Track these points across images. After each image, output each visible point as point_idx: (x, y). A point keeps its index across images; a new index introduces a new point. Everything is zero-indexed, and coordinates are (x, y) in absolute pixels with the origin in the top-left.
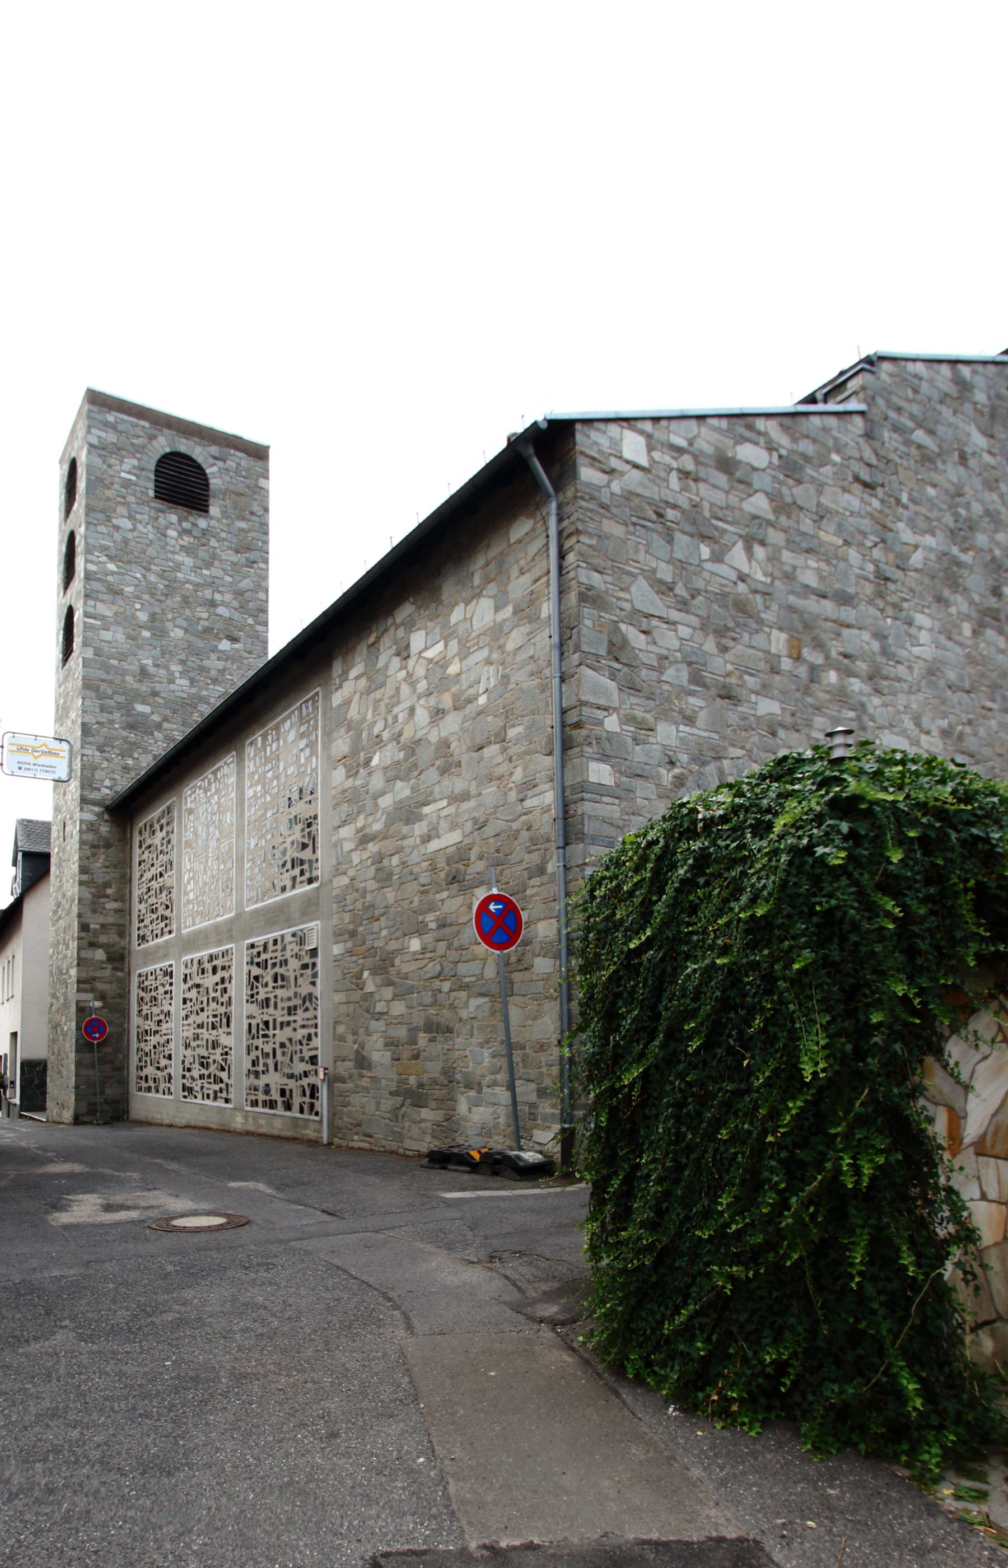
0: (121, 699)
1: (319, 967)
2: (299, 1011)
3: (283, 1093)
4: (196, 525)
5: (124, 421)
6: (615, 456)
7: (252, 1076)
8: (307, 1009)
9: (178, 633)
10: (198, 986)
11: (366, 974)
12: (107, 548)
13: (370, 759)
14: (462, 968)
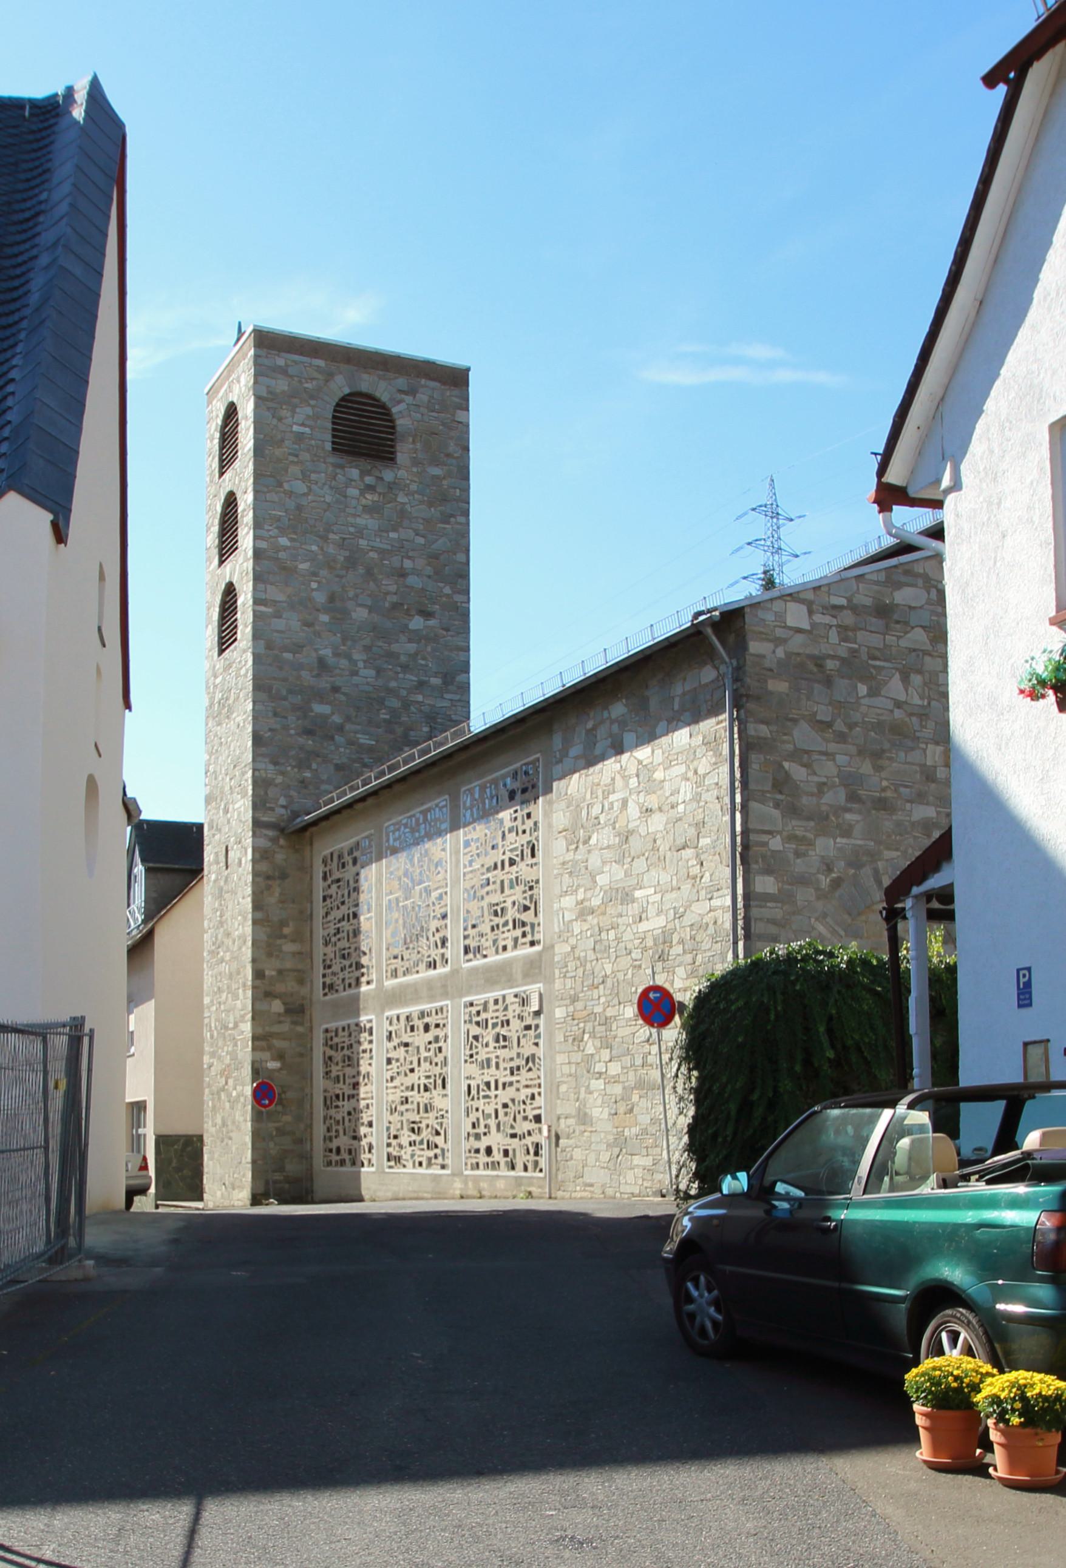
1: (541, 1029)
2: (523, 1071)
3: (506, 1153)
4: (382, 479)
5: (295, 362)
6: (780, 627)
7: (472, 1139)
8: (530, 1070)
9: (360, 614)
10: (406, 1045)
11: (586, 1036)
12: (278, 519)
13: (590, 838)
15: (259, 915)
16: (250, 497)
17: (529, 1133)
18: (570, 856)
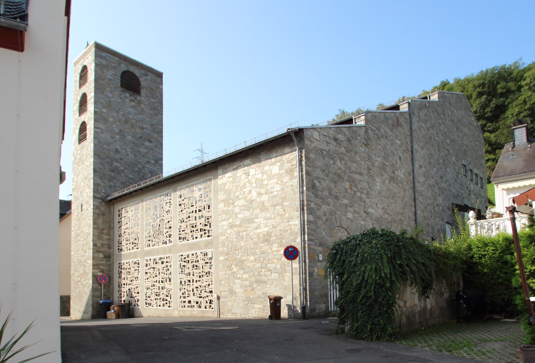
0: (109, 160)
1: (213, 263)
9: (129, 138)
11: (233, 266)
12: (103, 103)
14: (269, 265)
15: (95, 226)
16: (93, 94)
17: (207, 296)
18: (226, 208)
